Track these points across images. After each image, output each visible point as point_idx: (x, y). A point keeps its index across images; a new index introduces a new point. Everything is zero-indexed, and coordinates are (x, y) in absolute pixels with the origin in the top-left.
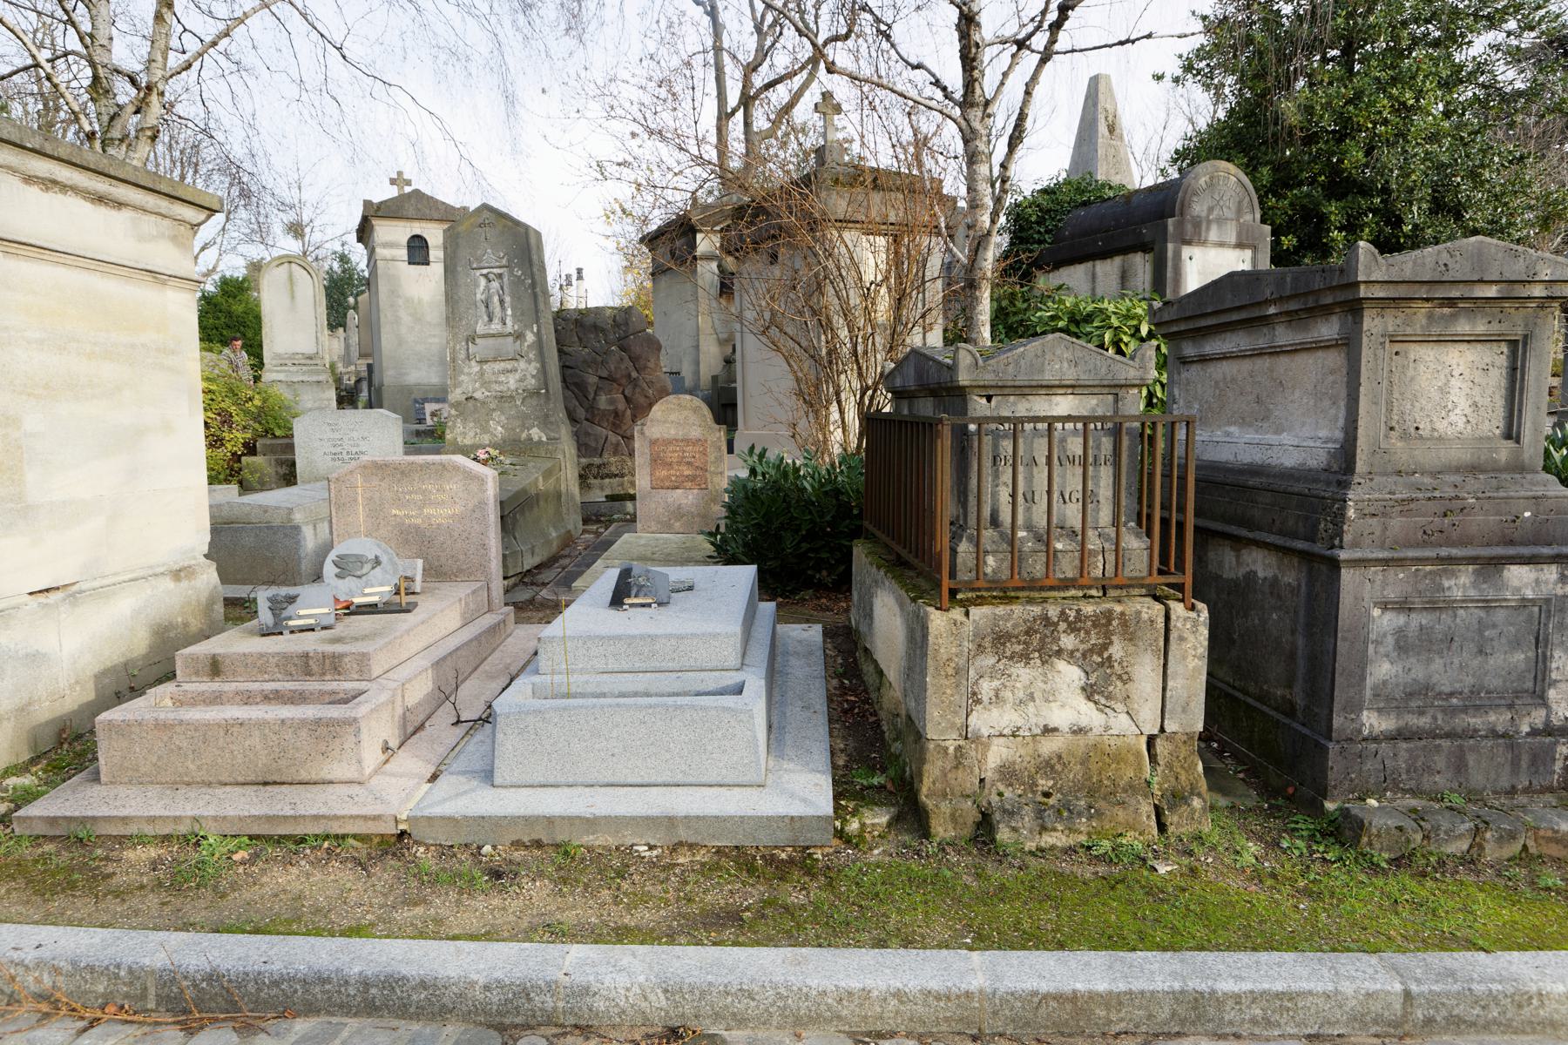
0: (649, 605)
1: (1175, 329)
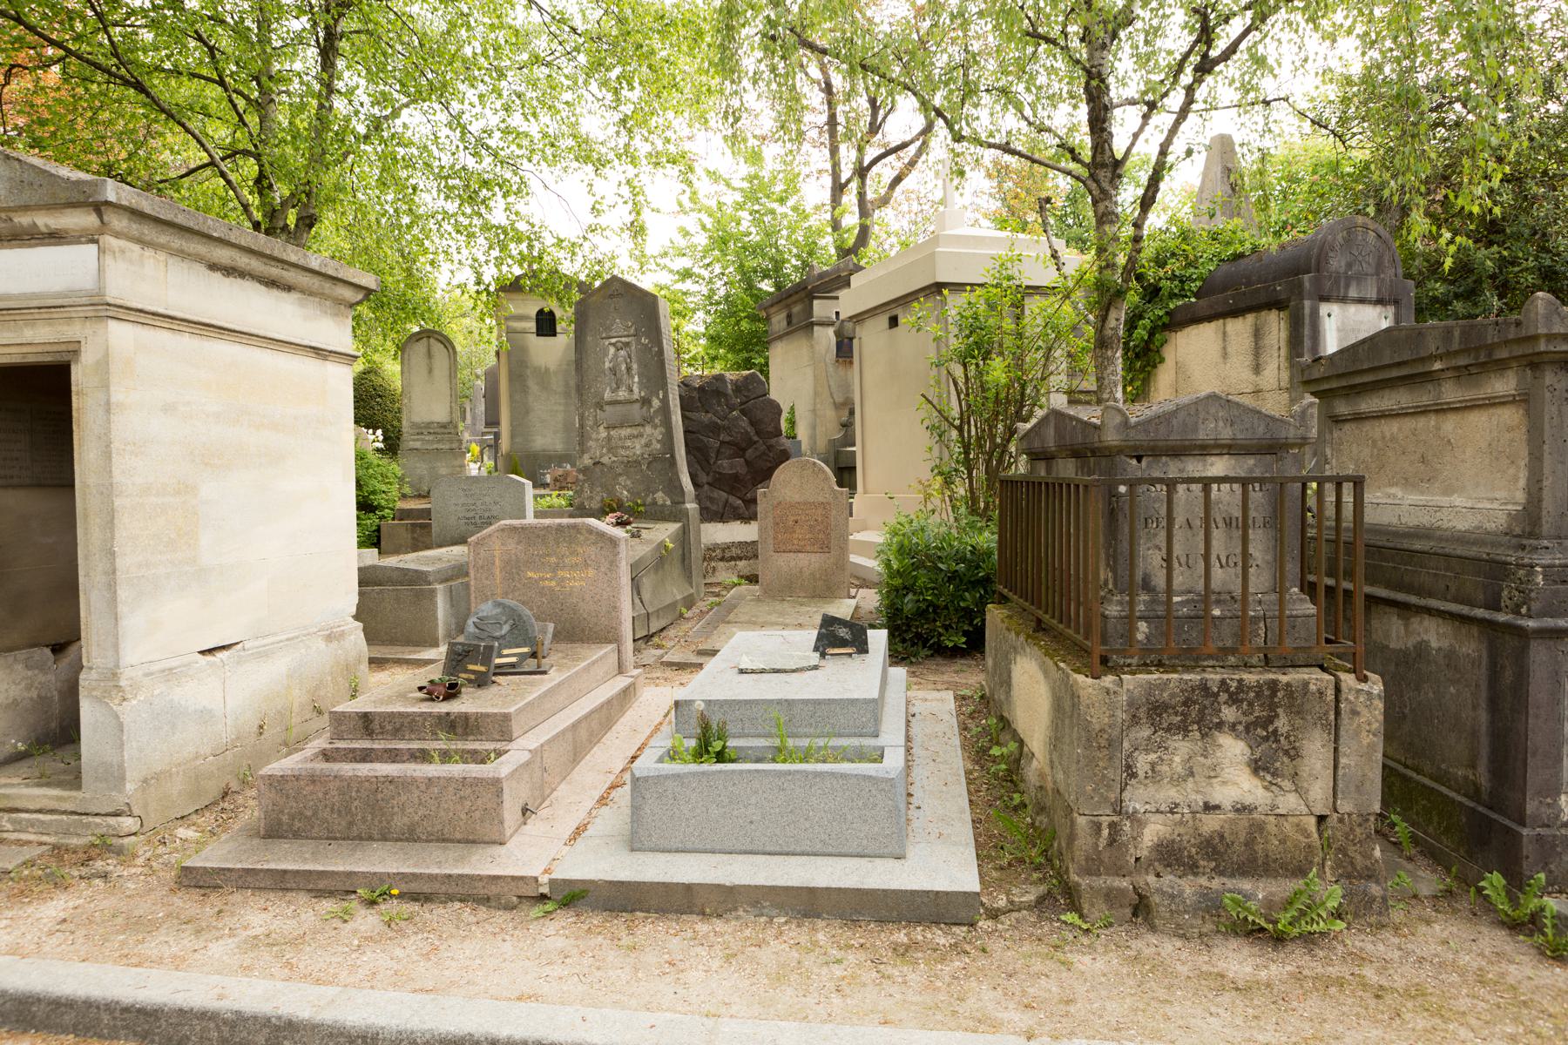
1: (1326, 386)
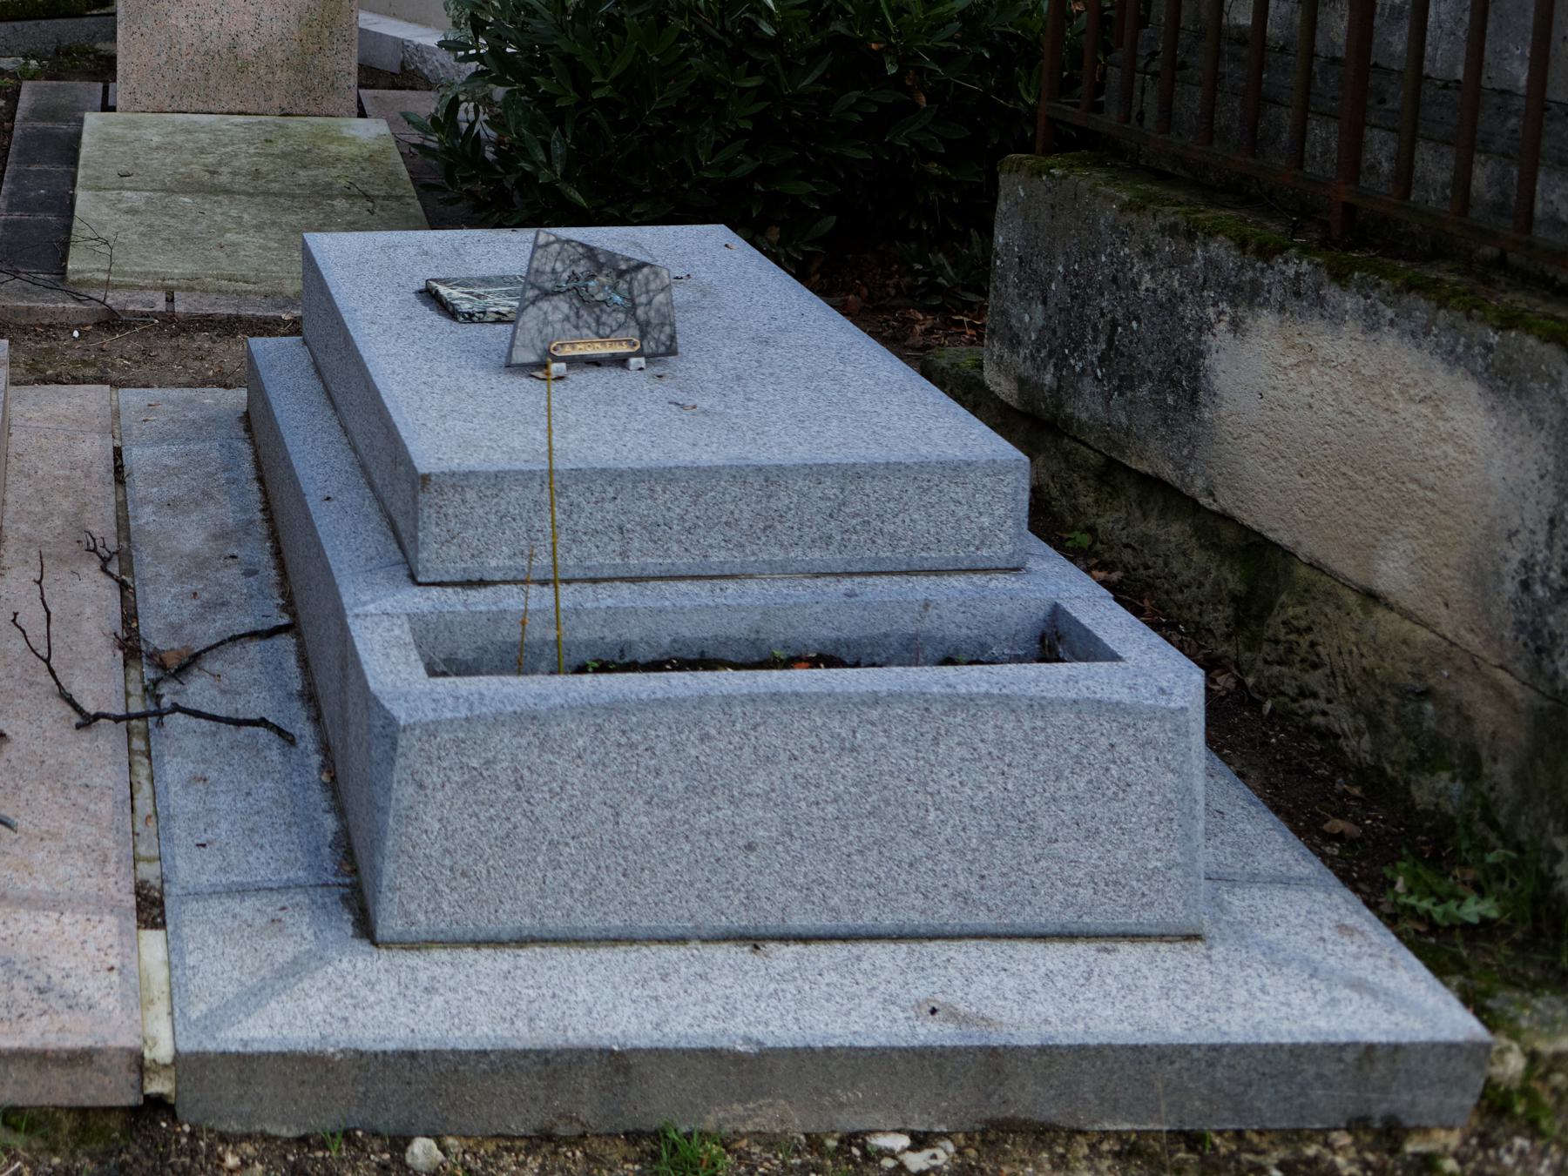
0: (620, 361)
